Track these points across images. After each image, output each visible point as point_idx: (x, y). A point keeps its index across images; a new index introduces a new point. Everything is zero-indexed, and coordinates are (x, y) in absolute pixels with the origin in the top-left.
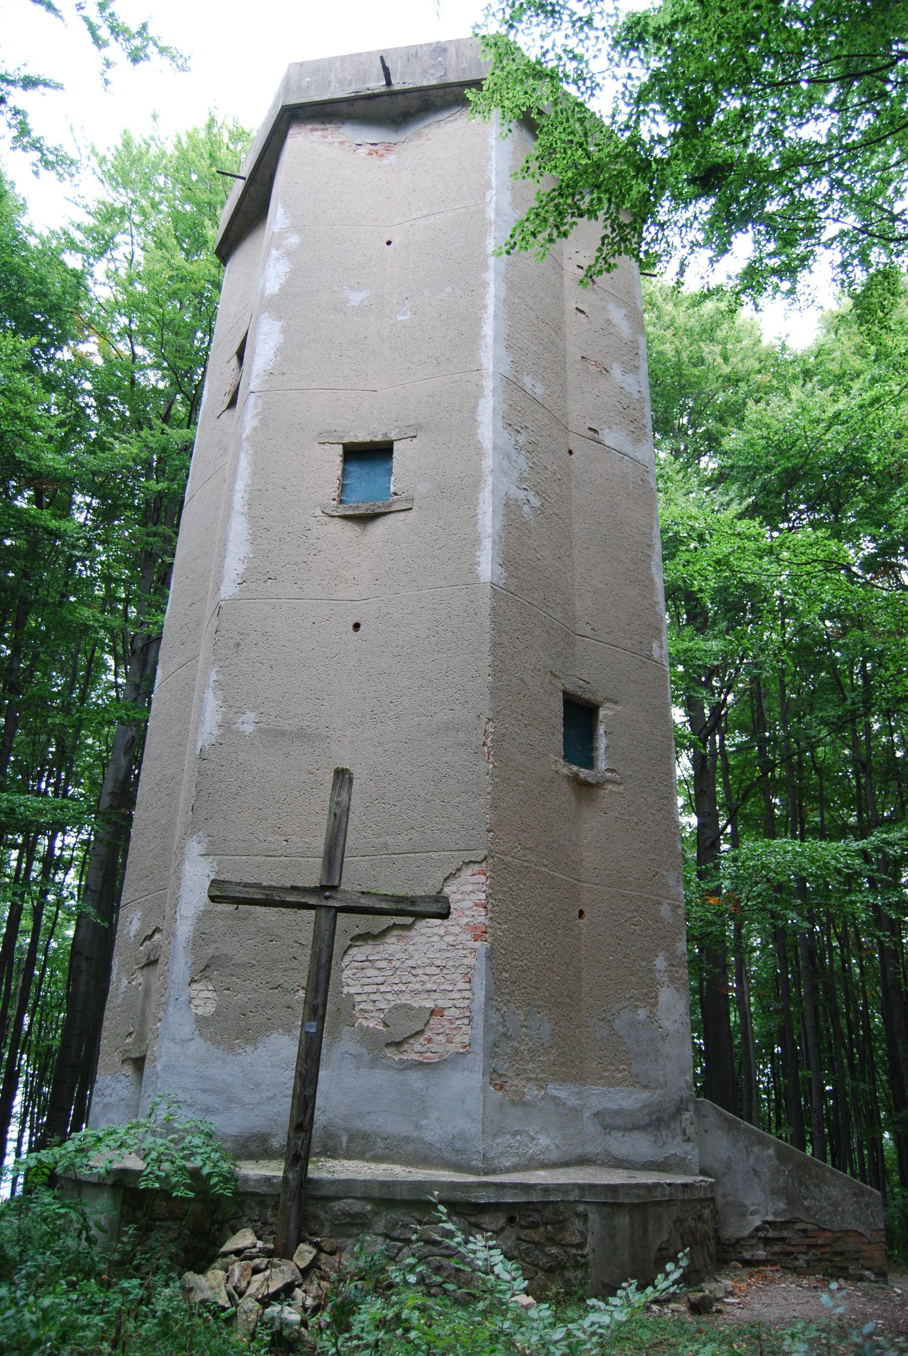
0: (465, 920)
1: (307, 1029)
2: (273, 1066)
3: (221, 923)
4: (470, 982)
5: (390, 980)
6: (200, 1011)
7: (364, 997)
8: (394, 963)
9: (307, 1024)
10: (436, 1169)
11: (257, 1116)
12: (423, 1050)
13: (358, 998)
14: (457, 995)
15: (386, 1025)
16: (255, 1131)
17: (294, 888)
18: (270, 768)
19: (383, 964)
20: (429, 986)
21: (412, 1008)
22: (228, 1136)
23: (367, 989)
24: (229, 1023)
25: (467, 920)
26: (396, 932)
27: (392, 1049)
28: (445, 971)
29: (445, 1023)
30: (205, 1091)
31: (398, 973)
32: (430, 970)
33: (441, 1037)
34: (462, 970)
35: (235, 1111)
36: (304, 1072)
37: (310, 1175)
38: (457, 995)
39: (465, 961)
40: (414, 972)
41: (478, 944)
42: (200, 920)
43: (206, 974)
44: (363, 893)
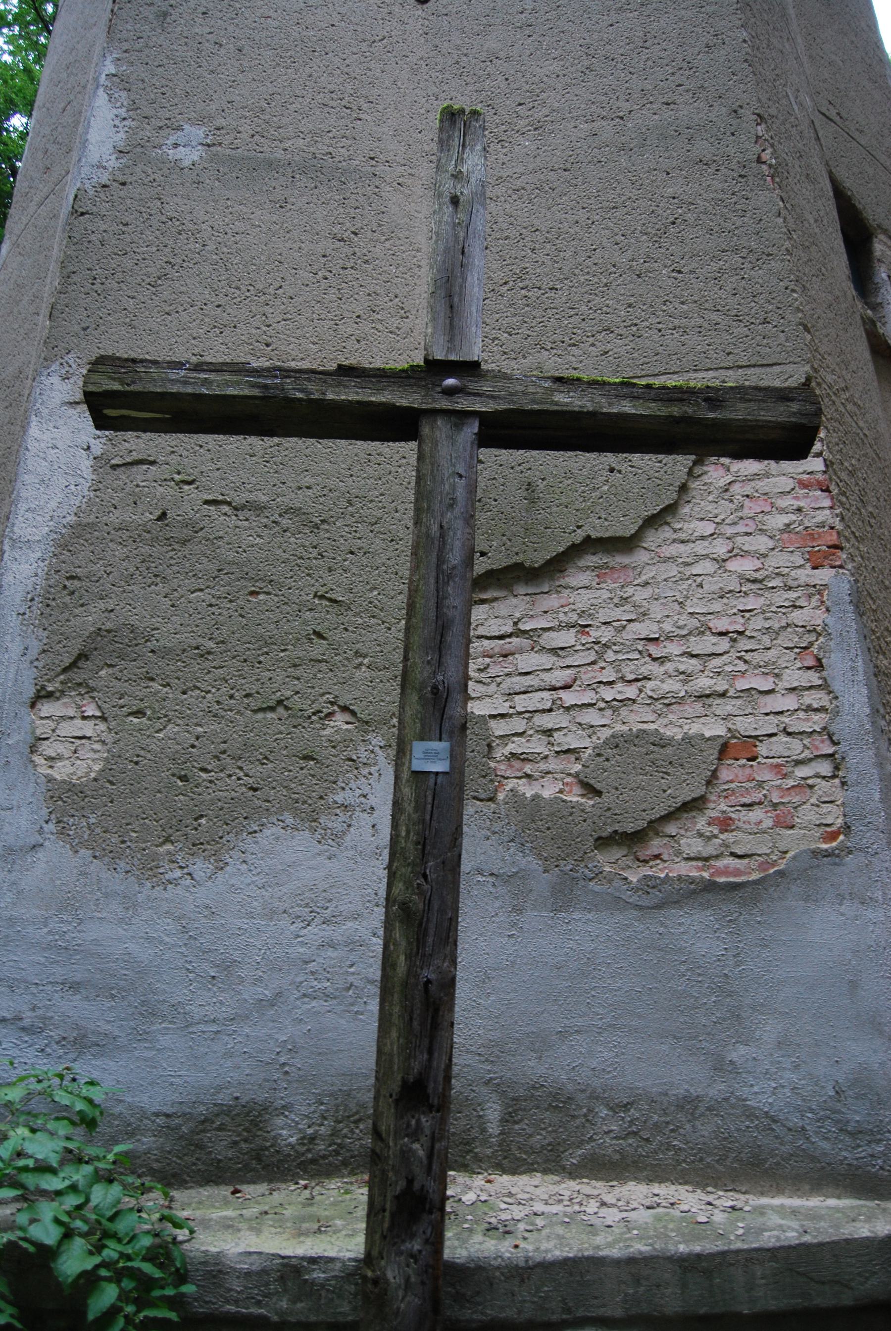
0: (779, 521)
1: (418, 765)
2: (271, 914)
3: (120, 552)
4: (819, 666)
5: (589, 676)
6: (62, 771)
7: (519, 725)
8: (594, 634)
9: (418, 748)
10: (797, 1192)
11: (229, 1055)
12: (710, 850)
13: (499, 728)
14: (790, 702)
15: (591, 790)
16: (224, 1098)
17: (345, 371)
18: (240, 226)
19: (566, 638)
20: (703, 683)
21: (662, 743)
22: (143, 1115)
23: (522, 703)
24: (142, 800)
25: (785, 519)
26: (590, 560)
27: (617, 853)
28: (744, 644)
29: (765, 775)
30: (75, 987)
31: (610, 656)
32: (706, 644)
33: (757, 814)
34: (788, 638)
35: (165, 1041)
36: (417, 901)
37: (447, 1254)
38: (790, 702)
39: (797, 616)
40: (655, 650)
41: (824, 575)
42: (65, 546)
43: (78, 676)
44: (559, 380)
